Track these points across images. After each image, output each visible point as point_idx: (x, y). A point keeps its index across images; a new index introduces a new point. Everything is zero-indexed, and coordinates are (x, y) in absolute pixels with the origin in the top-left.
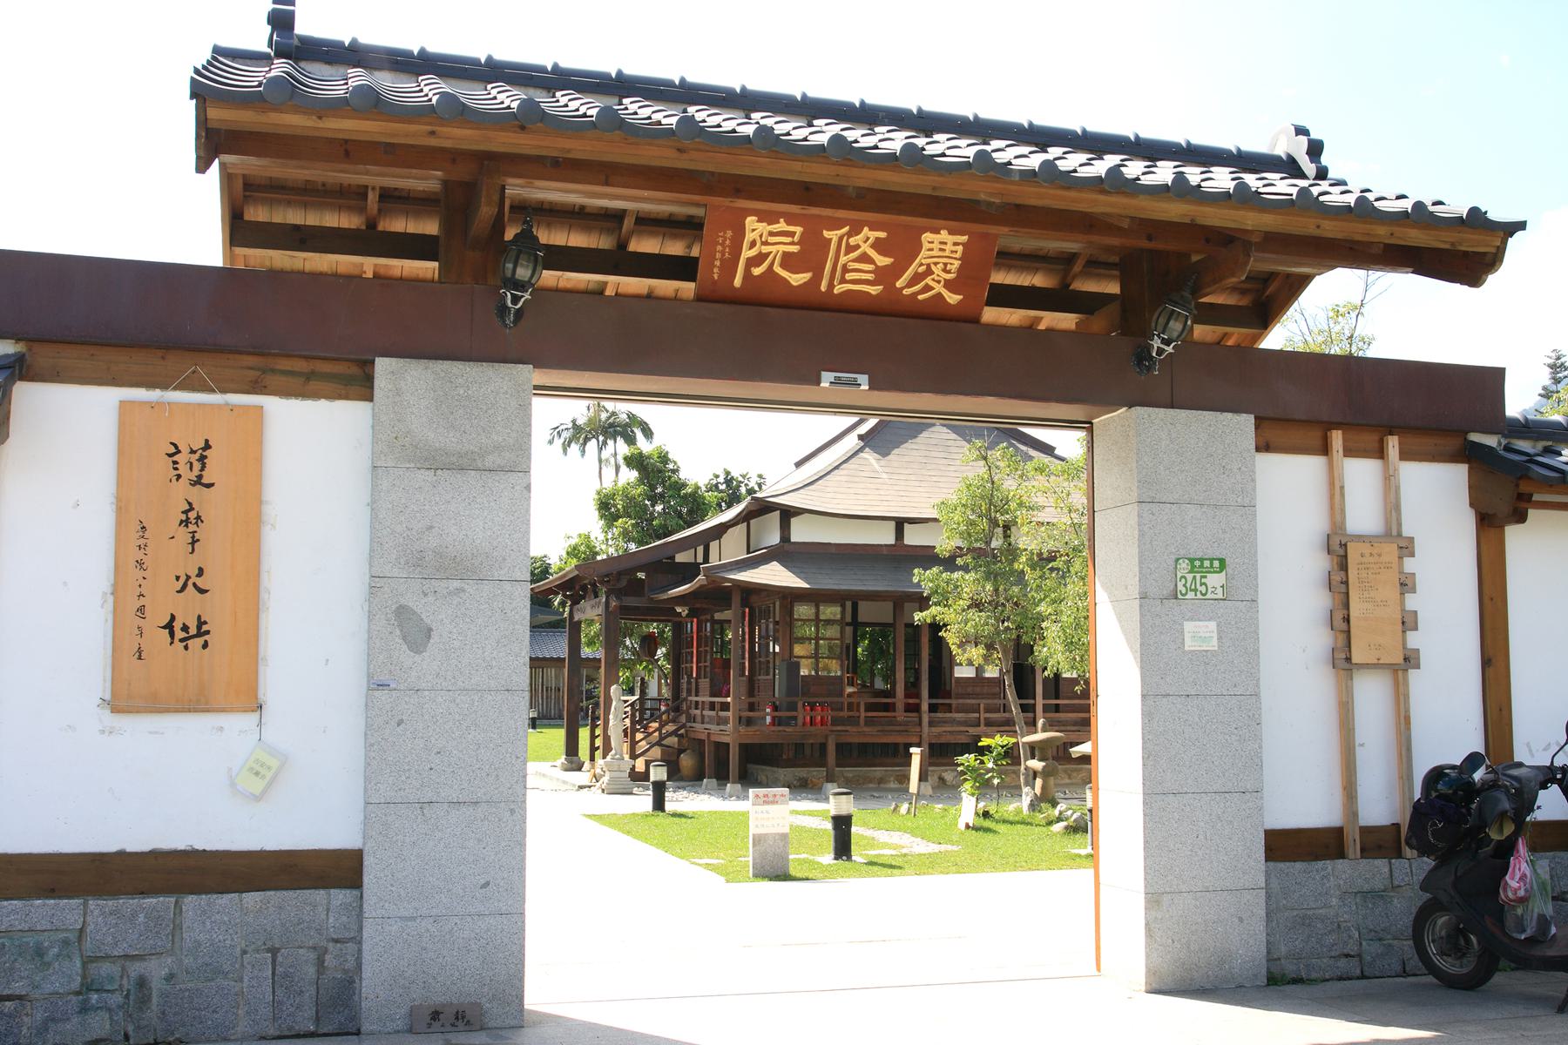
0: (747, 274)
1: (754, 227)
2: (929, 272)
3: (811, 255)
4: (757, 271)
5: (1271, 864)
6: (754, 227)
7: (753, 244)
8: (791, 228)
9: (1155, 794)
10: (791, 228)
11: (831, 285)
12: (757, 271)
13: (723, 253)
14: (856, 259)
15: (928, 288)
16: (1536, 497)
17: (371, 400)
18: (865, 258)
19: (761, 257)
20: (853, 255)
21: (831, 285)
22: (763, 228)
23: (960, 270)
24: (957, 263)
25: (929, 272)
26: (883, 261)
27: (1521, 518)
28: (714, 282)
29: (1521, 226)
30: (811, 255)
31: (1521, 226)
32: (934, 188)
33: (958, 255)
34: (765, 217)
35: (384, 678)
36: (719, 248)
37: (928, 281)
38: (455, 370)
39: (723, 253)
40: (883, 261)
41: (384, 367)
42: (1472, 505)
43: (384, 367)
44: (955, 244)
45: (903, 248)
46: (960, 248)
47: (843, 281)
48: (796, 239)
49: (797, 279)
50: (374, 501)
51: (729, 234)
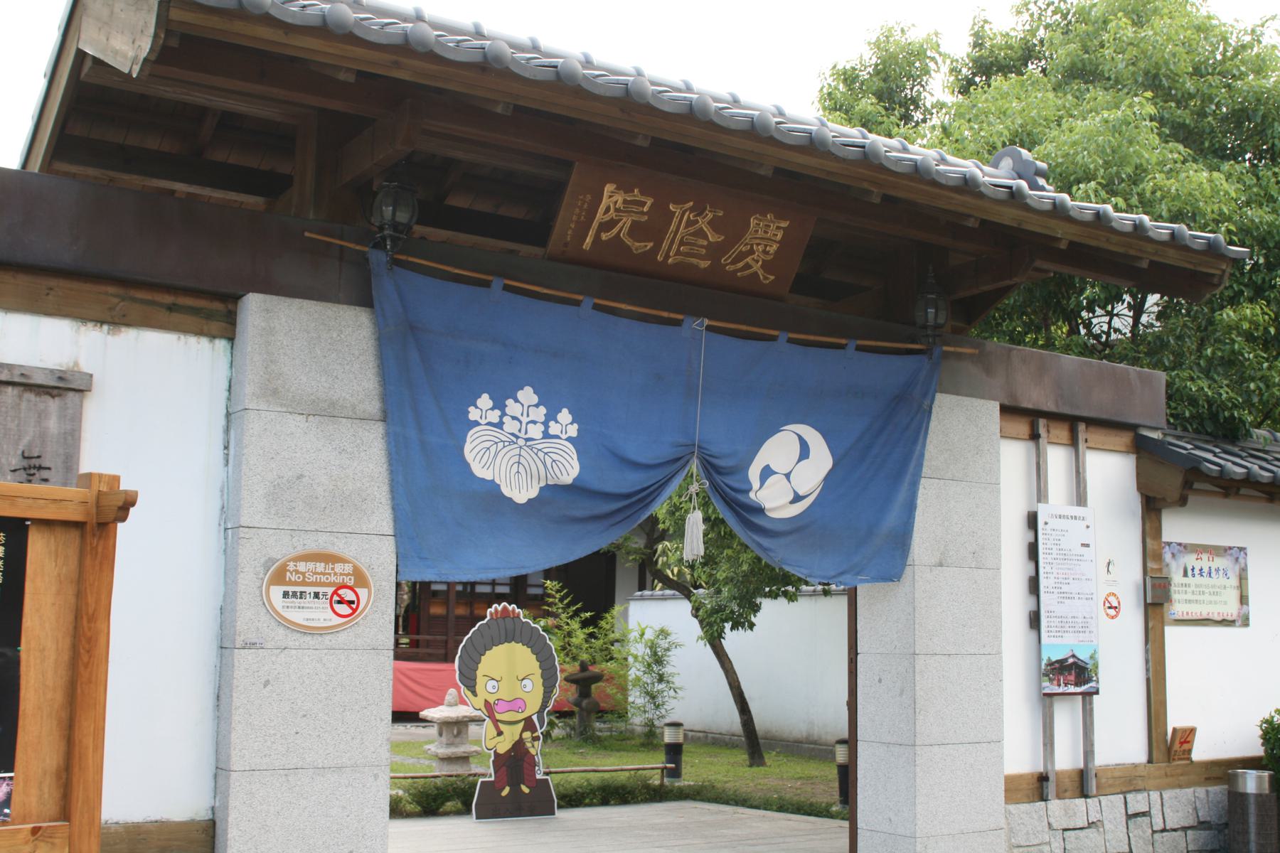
0: (597, 236)
1: (612, 197)
2: (752, 252)
3: (653, 229)
4: (604, 236)
5: (1012, 807)
6: (612, 197)
7: (608, 209)
8: (643, 199)
9: (175, 180)
10: (643, 199)
11: (667, 256)
12: (604, 236)
13: (579, 216)
14: (689, 233)
15: (748, 266)
16: (1196, 486)
17: (231, 339)
18: (700, 234)
19: (611, 224)
20: (692, 229)
22: (619, 198)
23: (776, 252)
24: (775, 247)
25: (752, 252)
26: (713, 237)
27: (1182, 502)
28: (566, 245)
30: (653, 229)
32: (829, 173)
33: (779, 237)
34: (624, 187)
36: (577, 211)
37: (749, 259)
38: (329, 313)
39: (579, 216)
40: (713, 237)
41: (254, 306)
42: (1139, 489)
43: (254, 306)
44: (778, 228)
45: (733, 230)
48: (645, 209)
50: (225, 551)
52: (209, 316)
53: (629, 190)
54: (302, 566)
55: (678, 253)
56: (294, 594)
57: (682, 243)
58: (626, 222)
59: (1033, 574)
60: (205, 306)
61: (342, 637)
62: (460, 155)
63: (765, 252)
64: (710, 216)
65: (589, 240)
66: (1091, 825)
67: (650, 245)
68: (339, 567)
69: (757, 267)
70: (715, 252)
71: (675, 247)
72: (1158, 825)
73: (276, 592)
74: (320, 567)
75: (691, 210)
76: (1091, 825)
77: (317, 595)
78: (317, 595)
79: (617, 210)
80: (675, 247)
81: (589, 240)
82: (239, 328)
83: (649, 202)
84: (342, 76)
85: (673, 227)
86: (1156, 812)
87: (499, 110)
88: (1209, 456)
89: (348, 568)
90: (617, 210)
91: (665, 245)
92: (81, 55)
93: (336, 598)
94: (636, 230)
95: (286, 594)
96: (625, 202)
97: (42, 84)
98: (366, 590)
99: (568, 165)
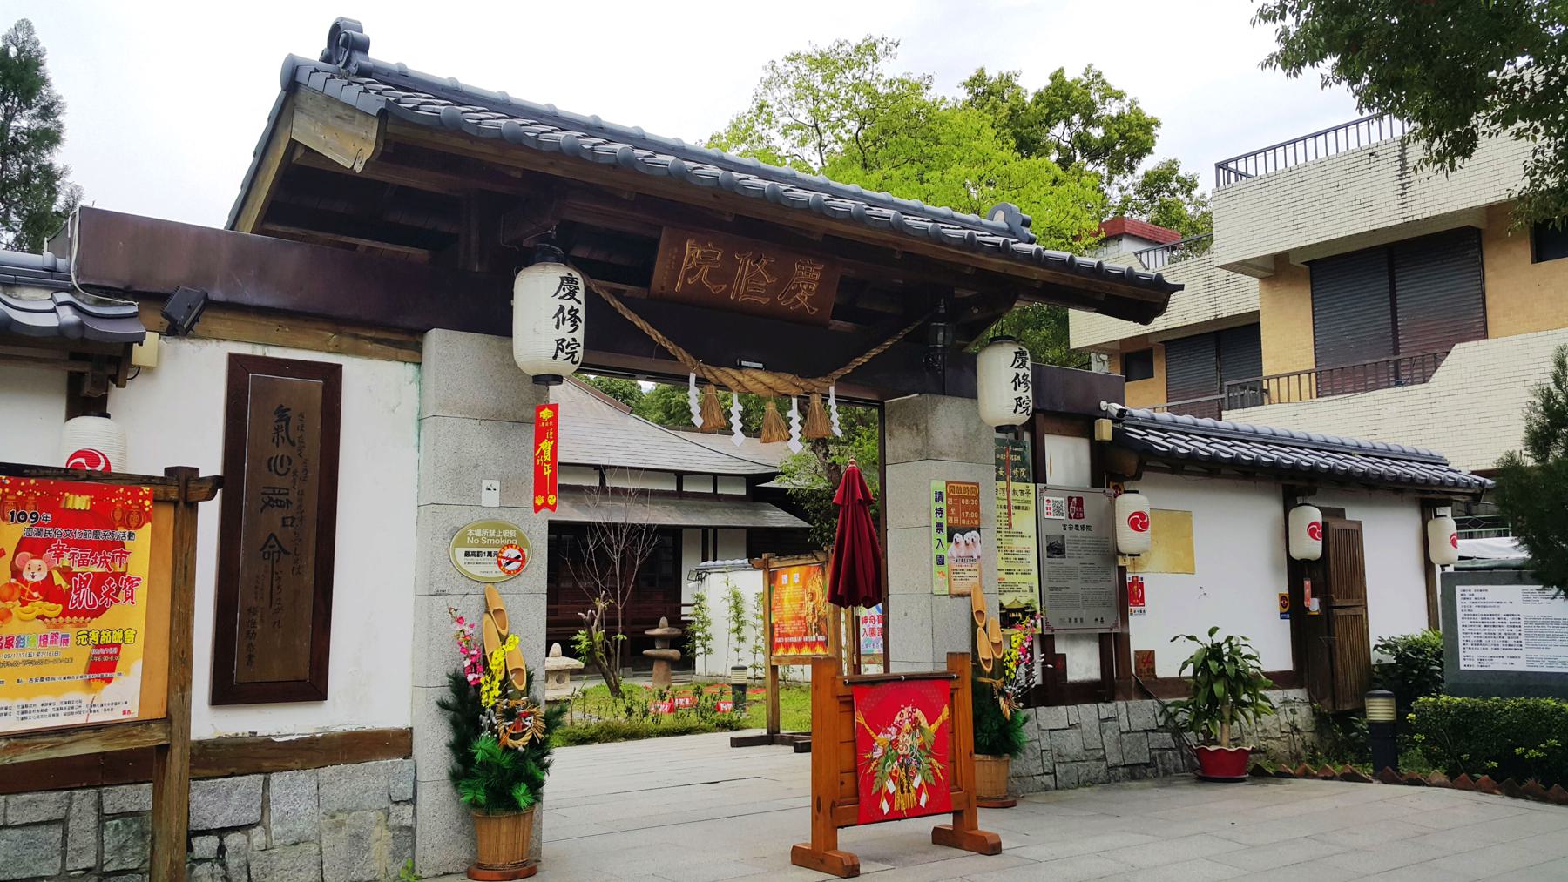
0: (685, 283)
3: (724, 275)
6: (692, 252)
14: (750, 281)
19: (692, 272)
29: (1181, 287)
31: (1181, 287)
35: (442, 587)
41: (436, 340)
43: (436, 340)
49: (717, 289)
52: (400, 345)
53: (705, 244)
54: (478, 533)
55: (745, 292)
56: (473, 554)
58: (705, 269)
59: (1430, 525)
60: (403, 340)
61: (508, 585)
62: (578, 219)
63: (808, 290)
66: (1071, 726)
68: (505, 533)
72: (1125, 727)
73: (460, 552)
74: (492, 533)
76: (1071, 726)
77: (490, 554)
78: (490, 554)
82: (599, 398)
84: (513, 174)
86: (1123, 717)
87: (625, 196)
88: (1159, 440)
89: (513, 533)
92: (293, 144)
93: (504, 562)
95: (467, 554)
97: (246, 161)
98: (1297, 554)
99: (661, 228)
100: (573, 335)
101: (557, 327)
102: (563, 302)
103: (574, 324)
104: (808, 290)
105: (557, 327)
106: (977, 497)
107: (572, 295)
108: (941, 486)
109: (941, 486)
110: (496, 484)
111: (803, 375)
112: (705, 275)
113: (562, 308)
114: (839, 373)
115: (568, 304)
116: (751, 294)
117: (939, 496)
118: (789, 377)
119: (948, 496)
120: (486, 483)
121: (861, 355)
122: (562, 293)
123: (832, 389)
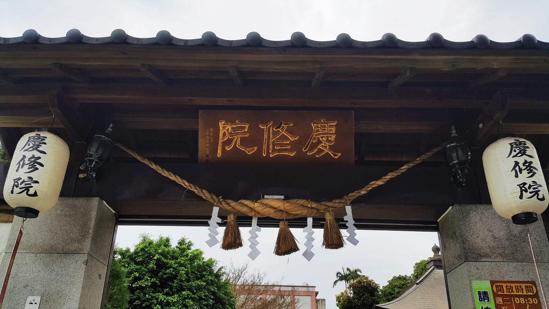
0: (223, 150)
2: (319, 142)
3: (255, 139)
6: (225, 128)
7: (224, 134)
11: (268, 154)
15: (320, 151)
18: (284, 138)
19: (228, 142)
21: (268, 154)
22: (229, 127)
28: (207, 156)
30: (255, 139)
46: (334, 130)
47: (274, 150)
49: (250, 151)
51: (212, 130)
53: (233, 122)
55: (274, 150)
57: (274, 145)
58: (237, 140)
64: (285, 127)
65: (219, 151)
67: (256, 148)
69: (326, 151)
70: (295, 146)
71: (271, 147)
75: (273, 126)
79: (230, 133)
80: (271, 147)
81: (219, 151)
83: (247, 126)
85: (265, 136)
90: (230, 133)
91: (265, 147)
94: (243, 141)
96: (232, 128)
100: (533, 179)
101: (517, 176)
102: (516, 159)
103: (530, 171)
104: (328, 141)
105: (517, 176)
106: (536, 296)
107: (523, 153)
108: (486, 286)
109: (486, 286)
110: (38, 299)
111: (317, 200)
112: (238, 142)
113: (517, 163)
114: (354, 195)
115: (521, 160)
116: (279, 150)
117: (483, 296)
118: (301, 202)
119: (495, 295)
120: (30, 299)
121: (377, 179)
122: (514, 153)
123: (349, 209)
